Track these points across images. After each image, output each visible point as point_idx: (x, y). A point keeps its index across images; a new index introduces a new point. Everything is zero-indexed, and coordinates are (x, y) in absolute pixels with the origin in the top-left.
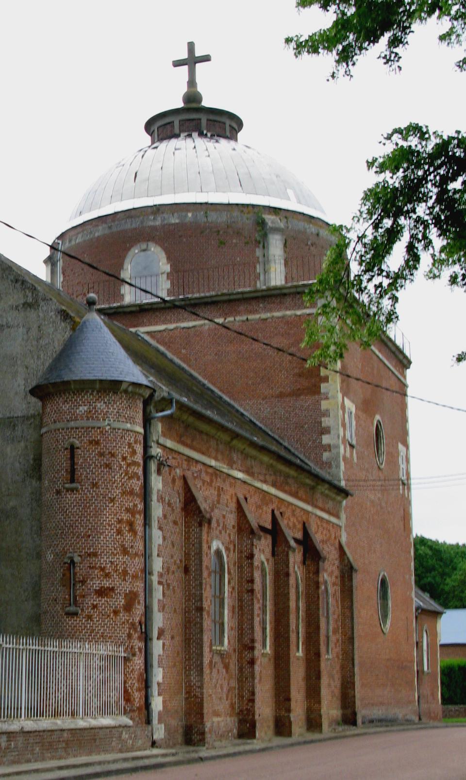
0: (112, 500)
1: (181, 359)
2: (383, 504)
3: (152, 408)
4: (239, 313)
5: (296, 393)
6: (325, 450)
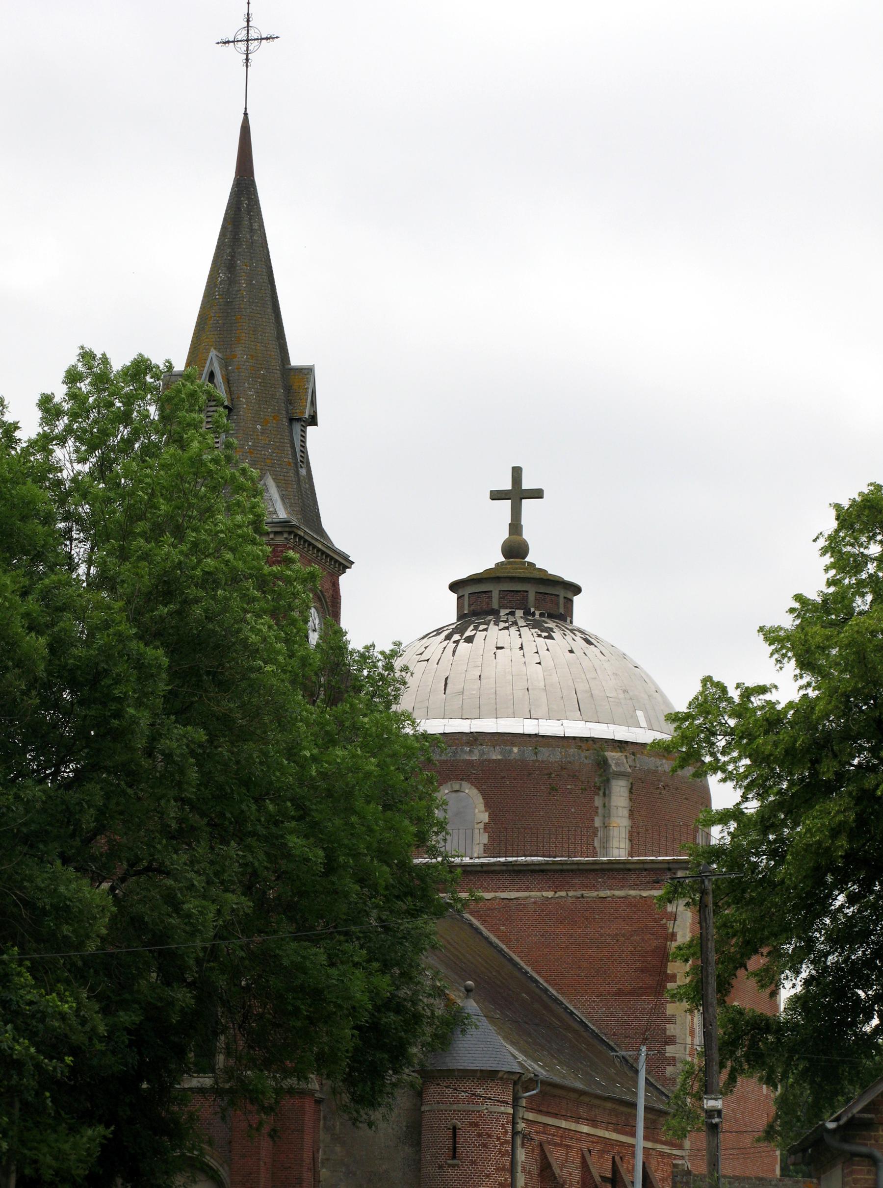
0: (488, 1176)
1: (498, 937)
2: (739, 1116)
3: (519, 1087)
4: (572, 887)
5: (636, 993)
6: (669, 1065)
